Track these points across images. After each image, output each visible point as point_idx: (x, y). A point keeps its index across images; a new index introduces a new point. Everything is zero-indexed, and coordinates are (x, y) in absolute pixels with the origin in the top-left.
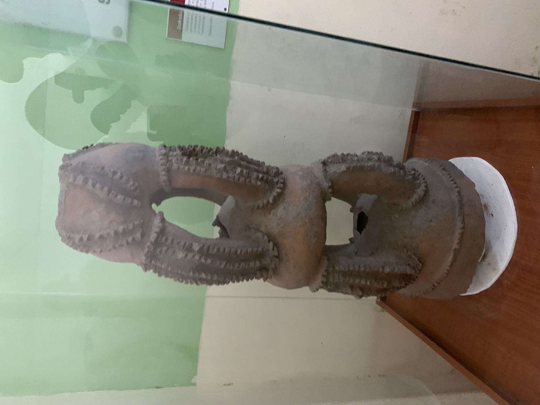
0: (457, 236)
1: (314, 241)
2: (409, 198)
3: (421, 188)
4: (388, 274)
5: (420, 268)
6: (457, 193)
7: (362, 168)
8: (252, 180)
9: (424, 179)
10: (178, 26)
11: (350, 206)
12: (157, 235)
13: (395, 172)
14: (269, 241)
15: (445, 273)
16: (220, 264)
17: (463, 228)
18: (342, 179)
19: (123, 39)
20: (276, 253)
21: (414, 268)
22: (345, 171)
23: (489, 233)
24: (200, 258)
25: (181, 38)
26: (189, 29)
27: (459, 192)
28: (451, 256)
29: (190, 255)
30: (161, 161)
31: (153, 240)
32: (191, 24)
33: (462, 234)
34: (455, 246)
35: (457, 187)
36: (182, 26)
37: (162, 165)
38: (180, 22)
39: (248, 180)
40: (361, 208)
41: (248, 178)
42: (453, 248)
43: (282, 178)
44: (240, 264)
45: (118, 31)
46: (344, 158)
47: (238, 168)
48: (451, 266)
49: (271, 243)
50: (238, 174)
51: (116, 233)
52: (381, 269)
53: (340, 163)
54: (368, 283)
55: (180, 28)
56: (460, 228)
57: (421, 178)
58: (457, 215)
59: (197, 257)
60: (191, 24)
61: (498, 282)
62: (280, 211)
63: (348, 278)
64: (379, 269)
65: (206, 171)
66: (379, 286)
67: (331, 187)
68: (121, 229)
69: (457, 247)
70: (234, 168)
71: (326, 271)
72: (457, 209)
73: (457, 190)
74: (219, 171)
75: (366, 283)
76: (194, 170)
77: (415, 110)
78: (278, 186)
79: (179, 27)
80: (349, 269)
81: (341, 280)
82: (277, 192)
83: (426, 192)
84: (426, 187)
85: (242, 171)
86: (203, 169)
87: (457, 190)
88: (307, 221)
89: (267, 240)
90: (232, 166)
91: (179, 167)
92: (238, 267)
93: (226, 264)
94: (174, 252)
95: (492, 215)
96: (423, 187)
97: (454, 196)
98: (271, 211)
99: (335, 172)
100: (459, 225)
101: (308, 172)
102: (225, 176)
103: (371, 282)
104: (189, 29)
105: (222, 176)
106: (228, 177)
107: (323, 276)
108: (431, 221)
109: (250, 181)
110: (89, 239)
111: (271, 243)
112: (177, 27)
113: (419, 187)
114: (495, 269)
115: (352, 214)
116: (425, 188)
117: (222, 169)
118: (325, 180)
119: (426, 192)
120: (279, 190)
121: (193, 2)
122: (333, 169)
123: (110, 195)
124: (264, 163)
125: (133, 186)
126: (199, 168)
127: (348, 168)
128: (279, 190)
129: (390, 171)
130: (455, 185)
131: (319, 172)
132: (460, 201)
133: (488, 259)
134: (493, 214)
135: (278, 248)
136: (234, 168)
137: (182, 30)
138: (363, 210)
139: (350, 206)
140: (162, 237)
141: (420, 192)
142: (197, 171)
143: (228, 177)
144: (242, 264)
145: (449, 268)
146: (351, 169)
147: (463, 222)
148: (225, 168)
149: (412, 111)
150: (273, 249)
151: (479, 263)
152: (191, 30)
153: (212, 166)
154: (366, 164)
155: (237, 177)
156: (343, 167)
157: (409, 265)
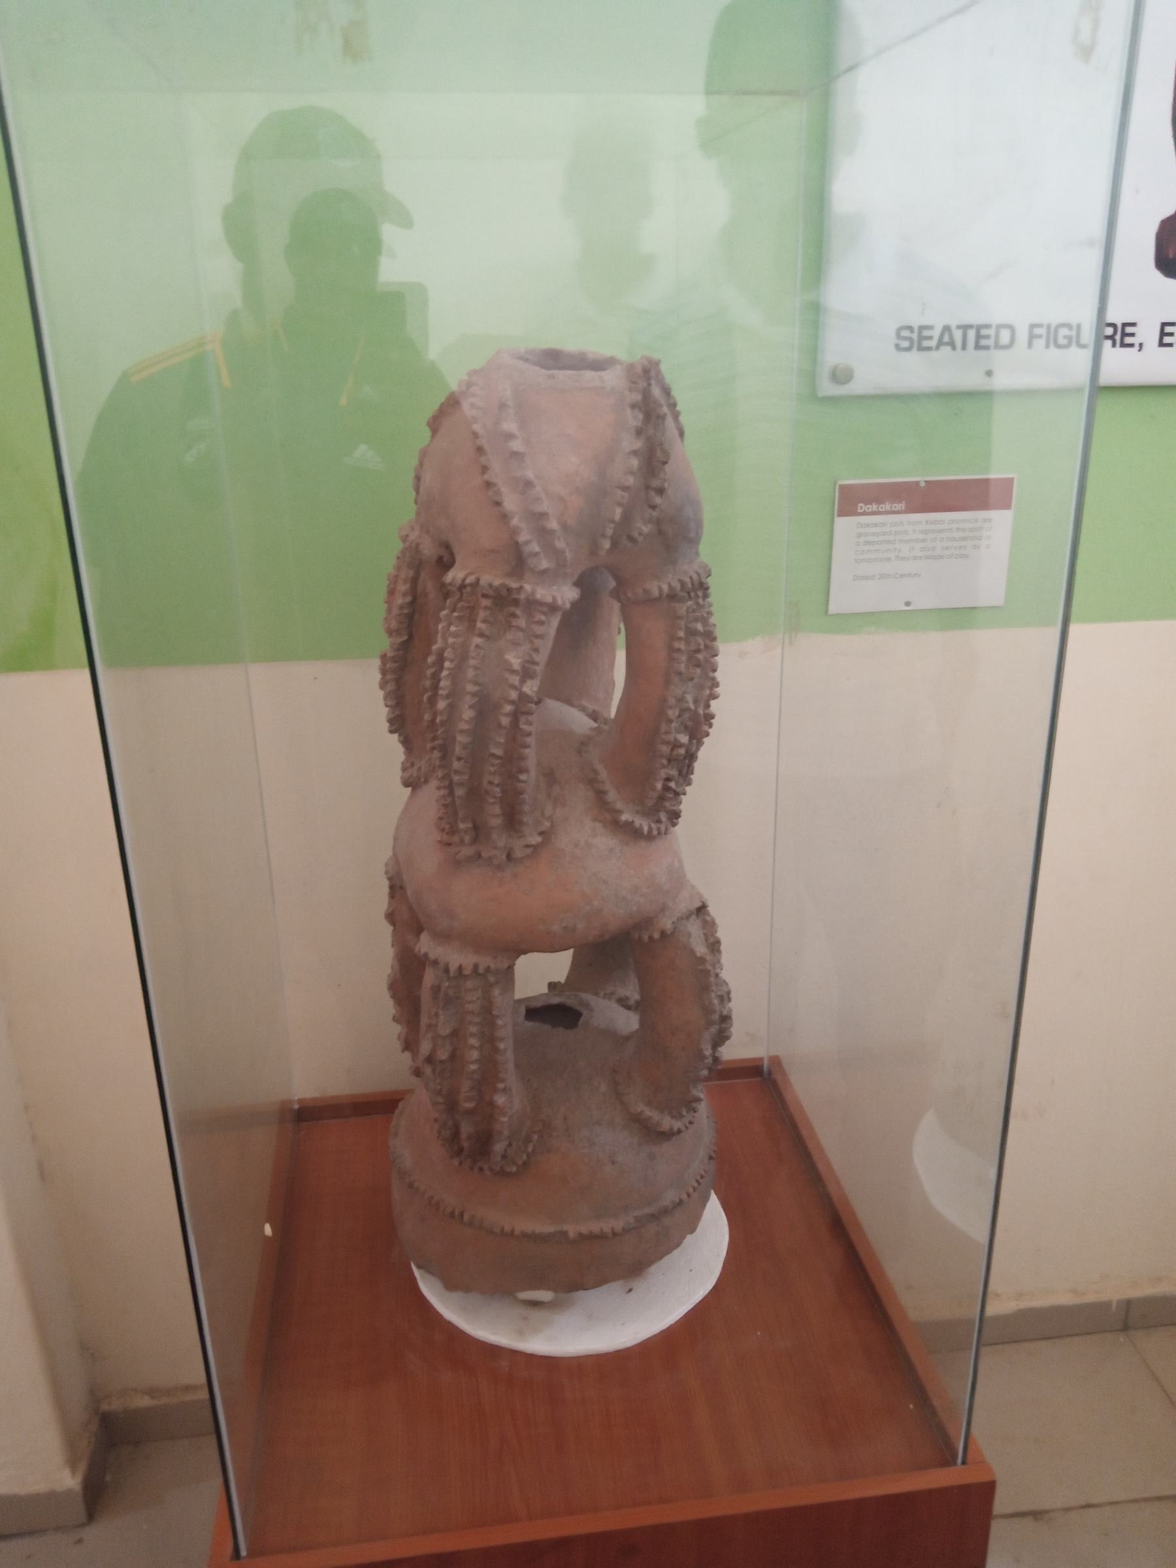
0: (595, 1227)
1: (555, 928)
2: (649, 1103)
3: (673, 1122)
4: (492, 1104)
5: (508, 1169)
6: (678, 1200)
7: (706, 988)
8: (666, 770)
9: (691, 1123)
10: (866, 505)
11: (562, 978)
12: (549, 603)
13: (704, 1057)
14: (541, 833)
15: (503, 1229)
16: (498, 744)
17: (615, 1234)
18: (679, 952)
19: (827, 388)
20: (518, 854)
21: (504, 1157)
22: (695, 956)
23: (591, 1298)
24: (512, 702)
25: (842, 513)
26: (862, 530)
27: (681, 1202)
28: (548, 1228)
29: (515, 680)
30: (687, 580)
31: (538, 596)
32: (873, 534)
33: (601, 1237)
34: (572, 1230)
35: (689, 1195)
36: (864, 514)
37: (680, 581)
38: (874, 507)
39: (665, 762)
40: (587, 1005)
41: (669, 760)
42: (565, 1227)
43: (666, 829)
44: (498, 785)
45: (841, 376)
46: (714, 946)
47: (686, 735)
48: (525, 1235)
49: (539, 839)
50: (676, 739)
51: (543, 515)
52: (501, 1086)
53: (706, 940)
54: (473, 1067)
55: (862, 511)
56: (613, 1229)
57: (688, 1117)
58: (637, 1213)
59: (514, 695)
60: (873, 534)
61: (494, 1351)
62: (604, 841)
63: (477, 1020)
64: (503, 1081)
65: (680, 674)
66: (466, 1092)
67: (663, 934)
68: (553, 524)
69: (571, 1235)
70: (686, 727)
71: (488, 969)
72: (648, 1210)
73: (684, 1197)
74: (681, 700)
75: (472, 1062)
76: (679, 650)
77: (766, 1063)
78: (653, 825)
79: (861, 507)
80: (497, 1017)
81: (470, 1007)
82: (641, 825)
83: (668, 1135)
84: (679, 1131)
85: (681, 745)
86: (682, 668)
87: (684, 1197)
88: (596, 903)
89: (543, 829)
90: (689, 724)
91: (680, 618)
92: (491, 783)
93: (498, 757)
94: (516, 644)
95: (630, 1290)
96: (677, 1125)
97: (670, 1197)
98: (600, 821)
99: (689, 935)
100: (618, 1224)
101: (678, 877)
102: (672, 713)
103: (474, 1072)
104: (862, 530)
105: (671, 708)
106: (670, 721)
107: (476, 966)
108: (613, 1163)
109: (664, 767)
110: (515, 454)
111: (539, 839)
112: (862, 505)
113: (673, 1117)
114: (521, 1333)
115: (545, 990)
116: (676, 1129)
117: (686, 705)
118: (675, 919)
119: (668, 1135)
120: (646, 829)
121: (915, 530)
122: (694, 928)
123: (620, 493)
124: (689, 784)
125: (640, 534)
126: (684, 658)
127: (702, 960)
128: (646, 829)
129: (704, 1047)
130: (691, 1190)
131: (684, 904)
132: (666, 1211)
133: (536, 1315)
134: (633, 1292)
135: (528, 857)
136: (686, 727)
137: (856, 514)
138: (585, 1012)
139: (562, 978)
140: (544, 614)
141: (667, 1122)
142: (676, 655)
143: (670, 721)
144: (498, 790)
145: (517, 1232)
146: (700, 967)
147: (626, 1231)
148: (688, 709)
149: (761, 1059)
150: (527, 846)
151: (515, 1298)
152: (860, 535)
153: (690, 684)
154: (713, 995)
155: (671, 738)
156: (701, 950)
157: (510, 1145)
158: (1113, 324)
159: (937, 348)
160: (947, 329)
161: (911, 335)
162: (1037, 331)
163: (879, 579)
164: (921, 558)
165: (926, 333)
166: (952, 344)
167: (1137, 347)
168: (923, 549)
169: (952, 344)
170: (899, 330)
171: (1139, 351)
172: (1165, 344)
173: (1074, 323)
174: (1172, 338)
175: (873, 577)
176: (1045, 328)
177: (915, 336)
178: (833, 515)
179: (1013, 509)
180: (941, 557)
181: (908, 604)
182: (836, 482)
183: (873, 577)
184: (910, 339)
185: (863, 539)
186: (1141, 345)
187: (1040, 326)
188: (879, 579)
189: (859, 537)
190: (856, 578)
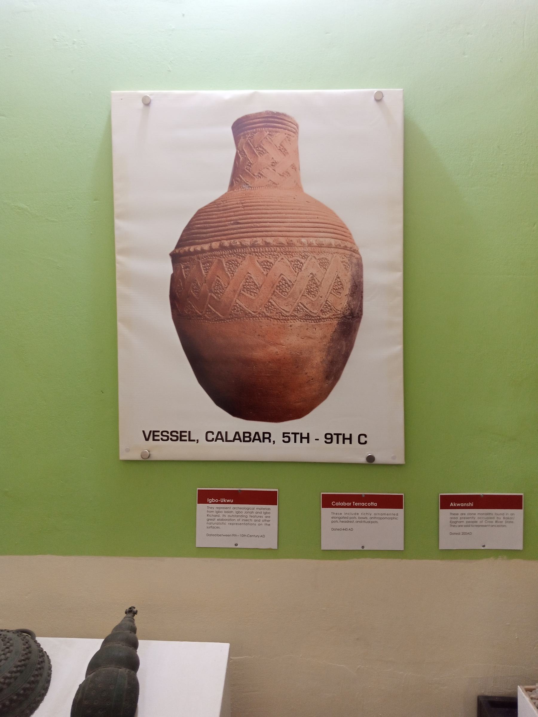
25: (443, 507)
38: (463, 505)
152: (208, 520)
158: (212, 432)
159: (233, 441)
160: (257, 433)
161: (167, 435)
162: (183, 434)
163: (462, 534)
164: (495, 526)
165: (183, 434)
166: (240, 439)
167: (196, 442)
168: (467, 522)
169: (240, 439)
170: (326, 435)
171: (274, 444)
172: (228, 440)
173: (342, 433)
174: (159, 437)
175: (459, 534)
176: (300, 434)
177: (179, 435)
178: (439, 509)
179: (523, 509)
180: (485, 526)
181: (363, 547)
182: (439, 494)
183: (459, 534)
184: (177, 436)
185: (210, 521)
186: (198, 440)
187: (186, 432)
188: (462, 534)
189: (208, 521)
190: (208, 535)
